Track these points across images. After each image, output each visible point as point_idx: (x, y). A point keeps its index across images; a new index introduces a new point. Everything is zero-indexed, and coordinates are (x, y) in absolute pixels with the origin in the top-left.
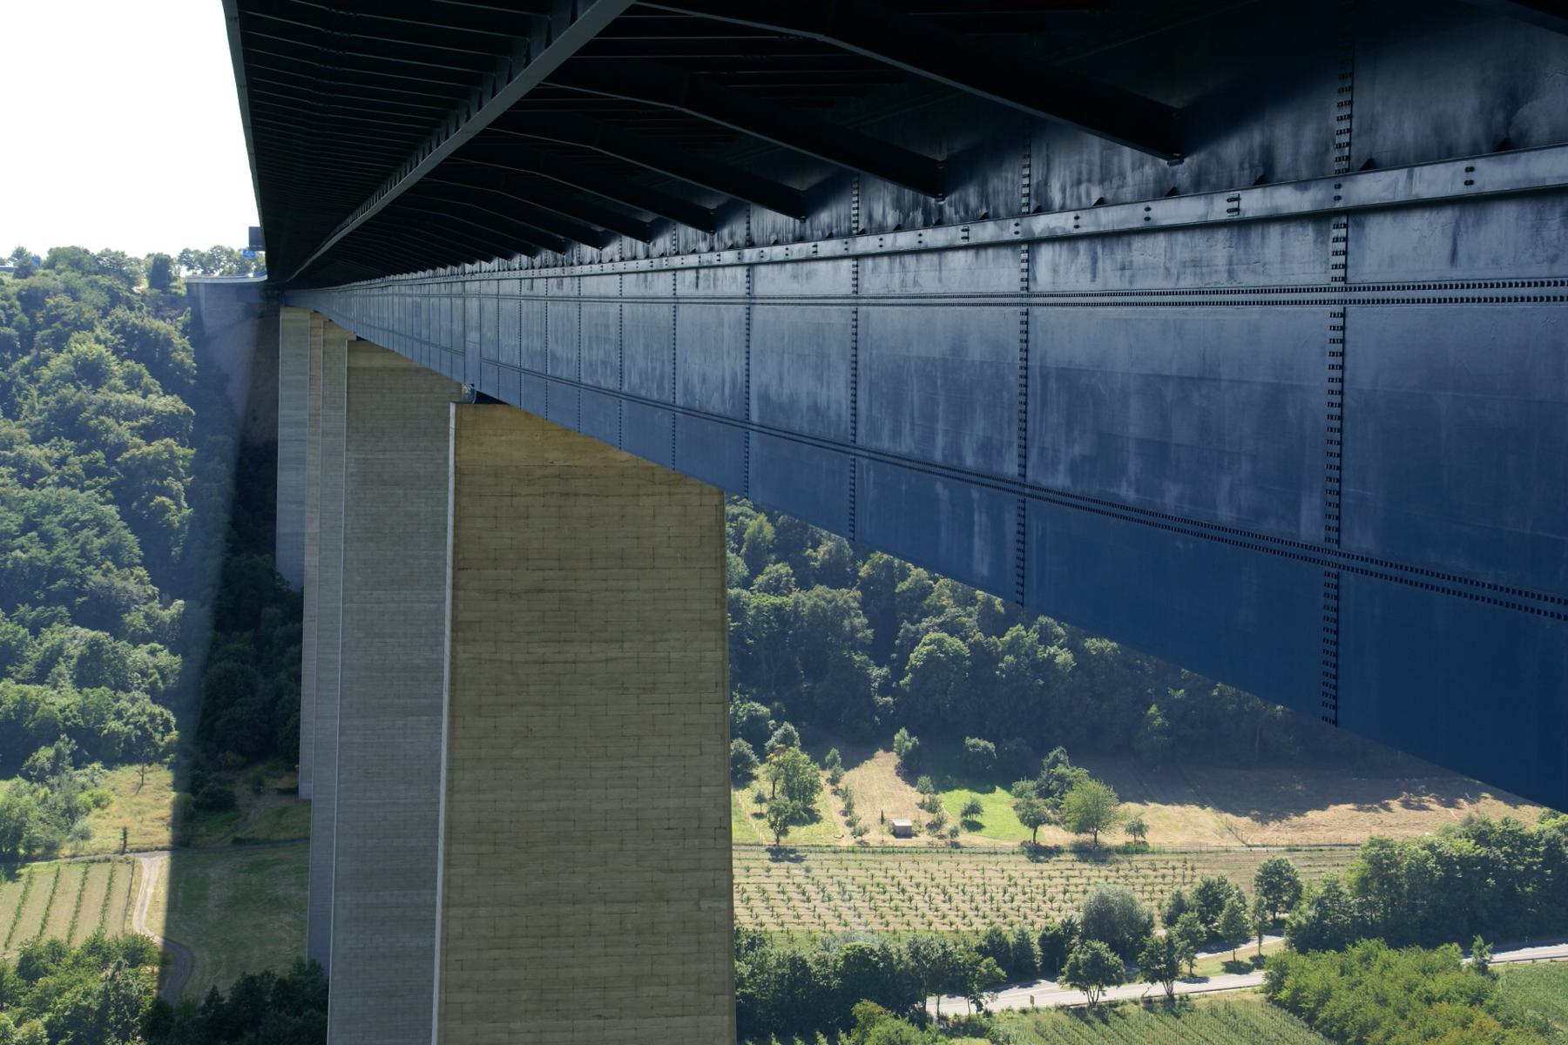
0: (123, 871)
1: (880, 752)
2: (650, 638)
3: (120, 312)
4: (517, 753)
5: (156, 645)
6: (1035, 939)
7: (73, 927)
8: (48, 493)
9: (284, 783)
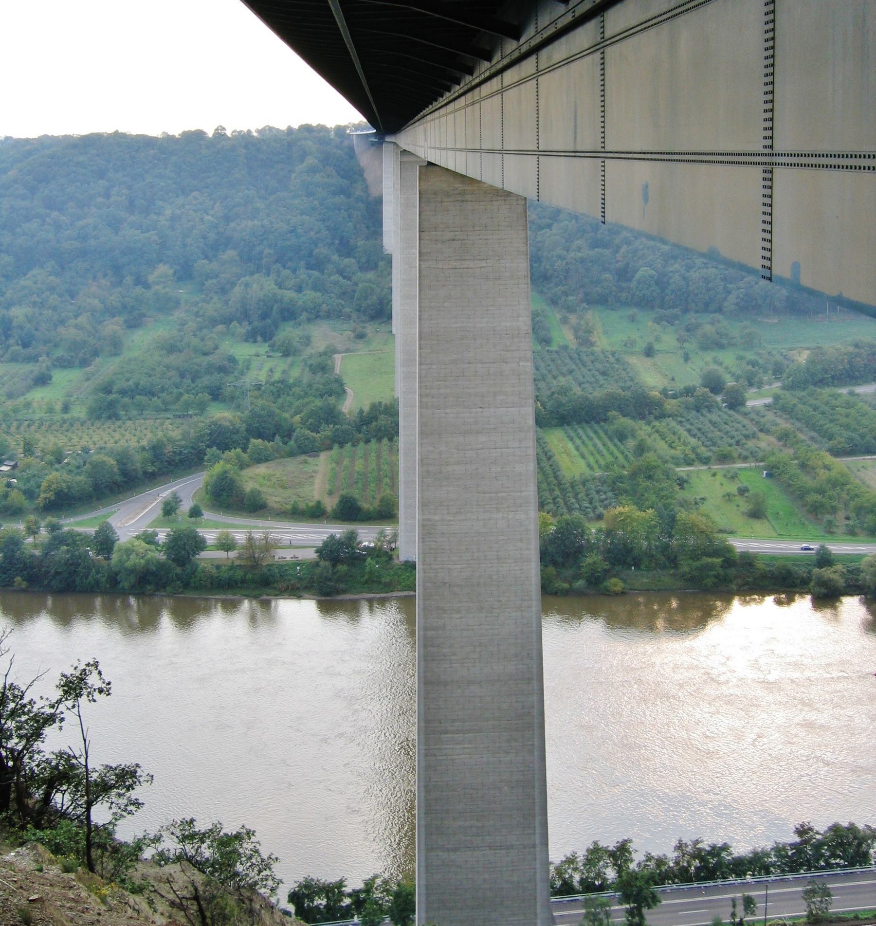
1: (229, 133)
2: (497, 258)
4: (446, 304)
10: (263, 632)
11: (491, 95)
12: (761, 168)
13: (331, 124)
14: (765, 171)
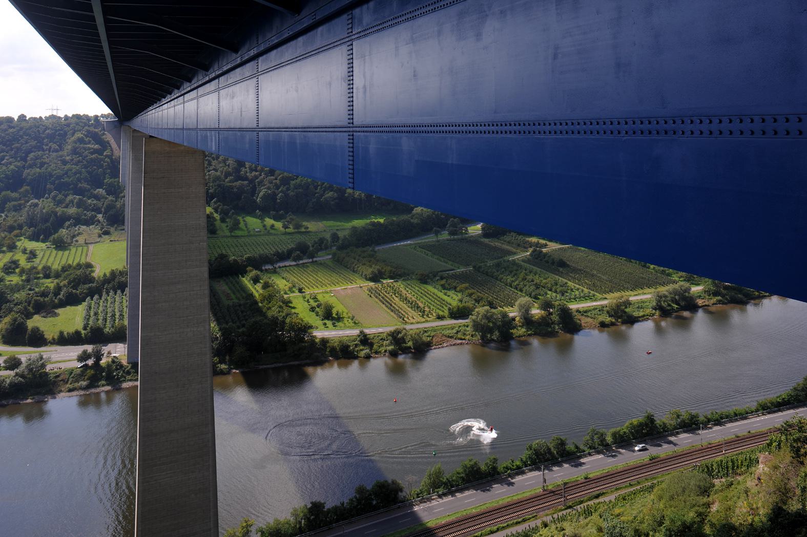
0: (85, 248)
3: (87, 128)
5: (93, 199)
6: (285, 251)
7: (74, 261)
8: (68, 167)
9: (122, 228)
10: (36, 424)
11: (192, 100)
12: (347, 134)
13: (91, 114)
14: (349, 135)
